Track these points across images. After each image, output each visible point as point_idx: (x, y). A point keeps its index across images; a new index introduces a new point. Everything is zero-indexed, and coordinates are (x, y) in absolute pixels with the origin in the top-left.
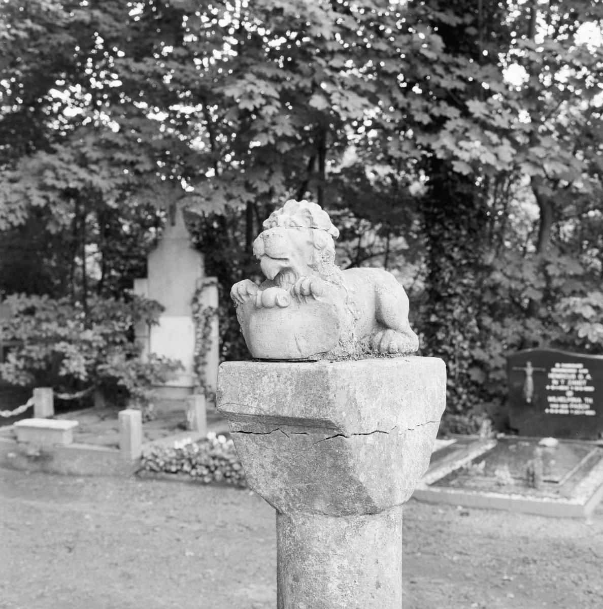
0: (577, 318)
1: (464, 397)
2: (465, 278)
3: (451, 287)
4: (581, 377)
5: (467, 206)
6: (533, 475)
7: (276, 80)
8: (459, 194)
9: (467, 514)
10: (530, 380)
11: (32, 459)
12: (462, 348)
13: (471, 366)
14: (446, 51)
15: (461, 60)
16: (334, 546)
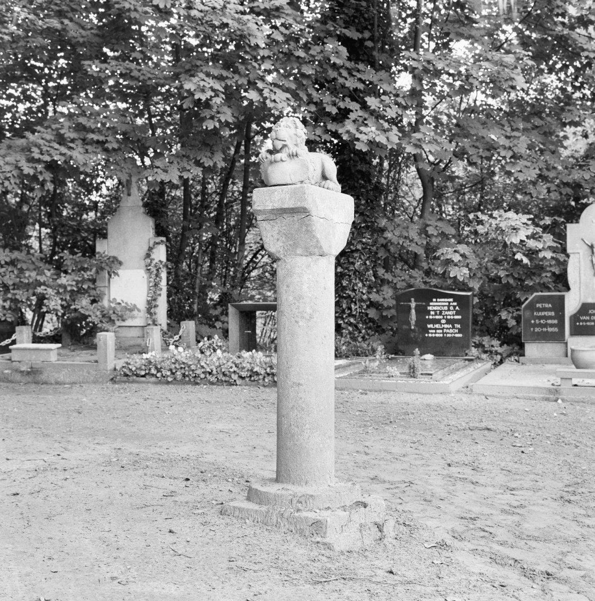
0: (449, 262)
1: (363, 331)
2: (364, 238)
3: (353, 245)
4: (452, 308)
5: (365, 181)
6: (414, 368)
7: (220, 78)
8: (360, 172)
9: (366, 394)
10: (413, 311)
11: (25, 373)
12: (362, 293)
13: (368, 307)
14: (349, 59)
15: (361, 66)
16: (305, 269)
